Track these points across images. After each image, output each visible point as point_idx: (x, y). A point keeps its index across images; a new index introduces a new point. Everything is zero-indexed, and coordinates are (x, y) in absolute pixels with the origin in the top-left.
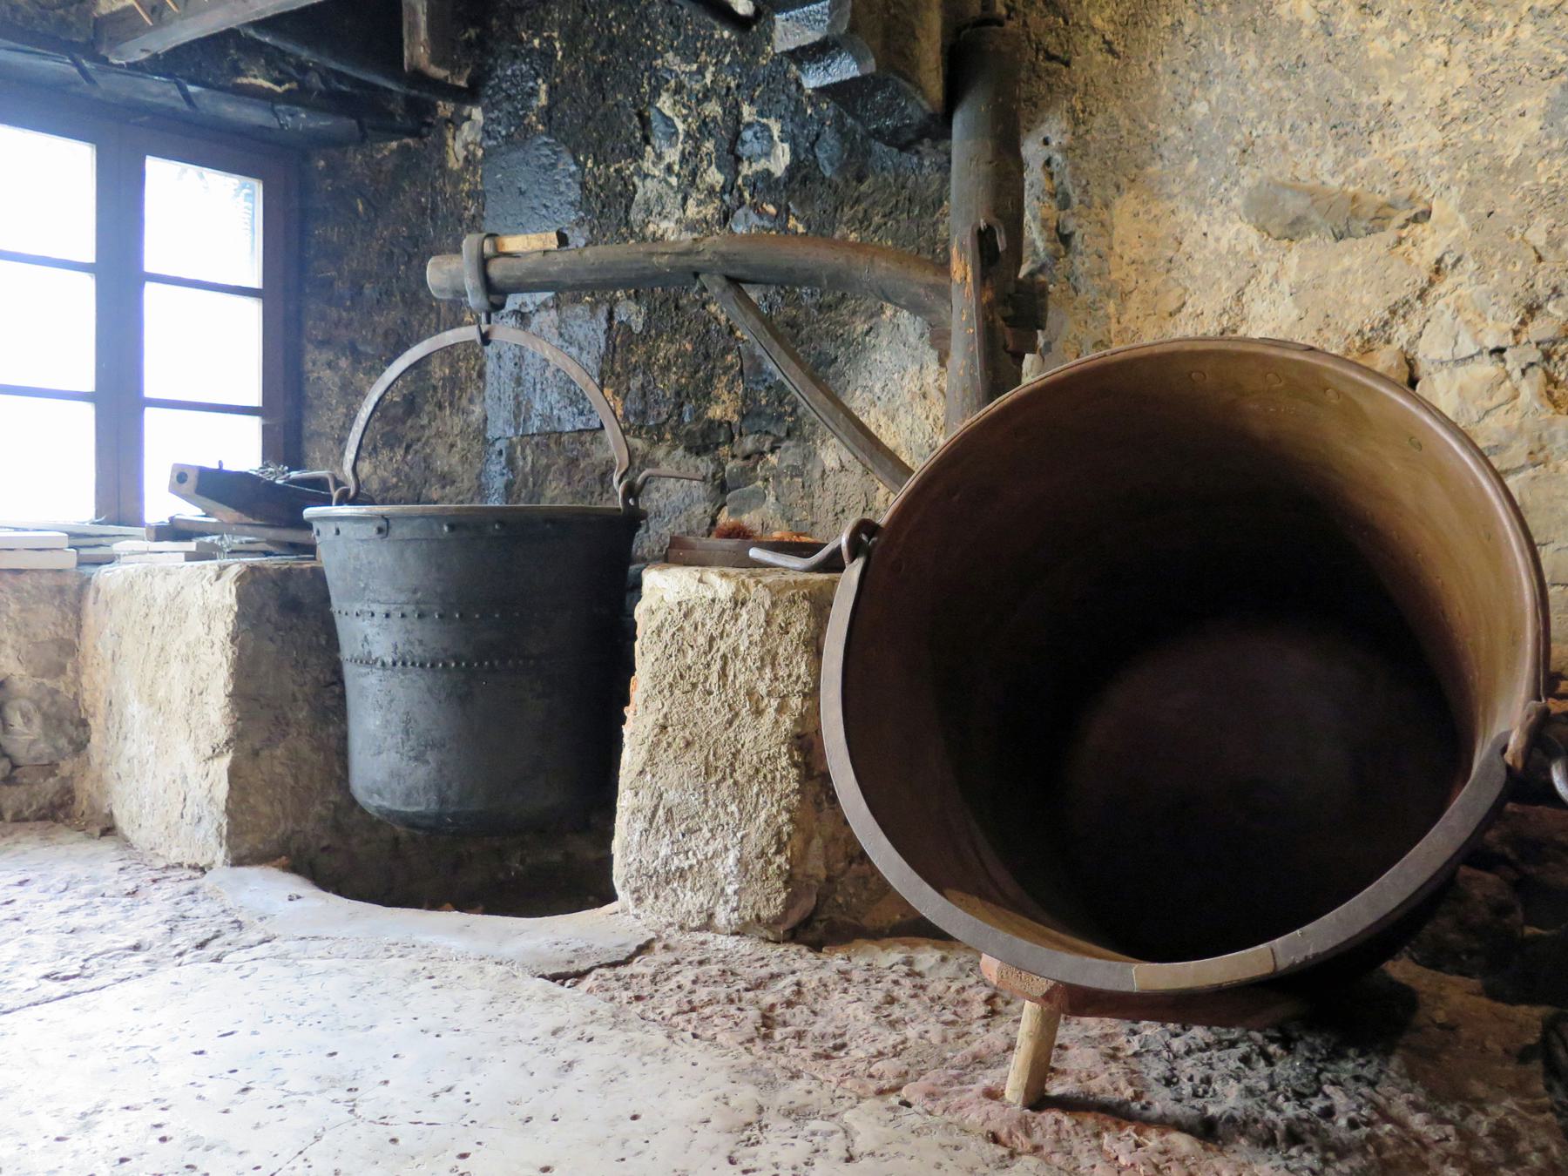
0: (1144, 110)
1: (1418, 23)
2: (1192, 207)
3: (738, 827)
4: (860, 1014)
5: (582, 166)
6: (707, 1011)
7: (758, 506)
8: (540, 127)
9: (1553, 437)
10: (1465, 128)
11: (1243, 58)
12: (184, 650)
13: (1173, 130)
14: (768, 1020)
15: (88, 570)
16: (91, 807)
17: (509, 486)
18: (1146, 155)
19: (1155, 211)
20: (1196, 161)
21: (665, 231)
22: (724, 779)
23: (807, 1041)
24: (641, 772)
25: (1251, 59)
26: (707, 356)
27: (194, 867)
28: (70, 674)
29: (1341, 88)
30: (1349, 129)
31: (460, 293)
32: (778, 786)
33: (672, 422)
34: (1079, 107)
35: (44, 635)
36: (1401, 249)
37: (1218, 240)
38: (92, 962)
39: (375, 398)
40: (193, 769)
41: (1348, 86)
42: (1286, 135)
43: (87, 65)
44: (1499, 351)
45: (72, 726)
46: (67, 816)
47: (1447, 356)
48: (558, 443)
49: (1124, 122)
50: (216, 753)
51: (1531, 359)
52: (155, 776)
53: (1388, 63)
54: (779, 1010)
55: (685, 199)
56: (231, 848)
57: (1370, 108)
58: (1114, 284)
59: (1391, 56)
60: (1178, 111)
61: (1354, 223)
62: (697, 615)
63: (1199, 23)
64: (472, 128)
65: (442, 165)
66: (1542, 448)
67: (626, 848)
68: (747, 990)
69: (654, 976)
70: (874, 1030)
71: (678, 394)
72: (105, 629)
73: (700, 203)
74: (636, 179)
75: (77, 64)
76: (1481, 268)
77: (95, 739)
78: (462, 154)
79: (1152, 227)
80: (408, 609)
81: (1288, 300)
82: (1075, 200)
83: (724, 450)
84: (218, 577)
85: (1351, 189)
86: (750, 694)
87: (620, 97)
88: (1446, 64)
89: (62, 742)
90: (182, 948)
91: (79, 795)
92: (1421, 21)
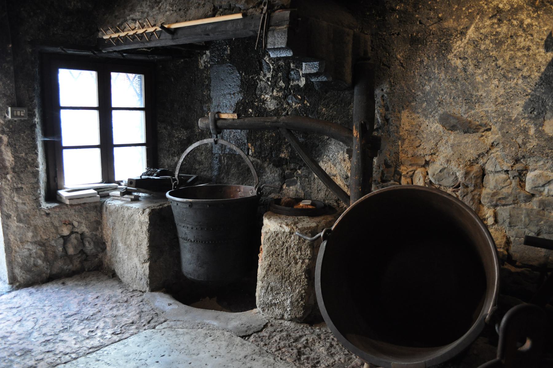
1: (491, 73)
2: (424, 117)
3: (291, 293)
4: (323, 351)
6: (283, 350)
9: (520, 197)
10: (502, 106)
11: (440, 75)
12: (134, 232)
13: (419, 93)
14: (300, 353)
15: (103, 200)
16: (108, 266)
17: (220, 168)
18: (411, 99)
19: (413, 117)
21: (267, 98)
22: (287, 280)
23: (310, 361)
24: (264, 277)
25: (442, 76)
26: (280, 138)
27: (141, 291)
31: (208, 129)
34: (392, 81)
35: (92, 220)
36: (482, 138)
37: (431, 128)
38: (123, 328)
39: (184, 157)
40: (139, 265)
42: (452, 100)
44: (507, 172)
45: (101, 244)
47: (493, 170)
48: (234, 157)
49: (405, 88)
50: (145, 262)
51: (515, 175)
52: (128, 265)
53: (482, 83)
54: (302, 349)
55: (273, 90)
57: (476, 96)
58: (400, 136)
59: (482, 82)
60: (421, 88)
61: (470, 130)
62: (280, 235)
64: (206, 57)
65: (198, 66)
66: (517, 200)
67: (260, 297)
68: (294, 342)
69: (269, 336)
70: (327, 357)
71: (271, 148)
72: (108, 221)
76: (504, 147)
77: (108, 248)
78: (203, 65)
79: (412, 121)
80: (198, 227)
82: (390, 109)
84: (143, 213)
86: (294, 258)
87: (253, 55)
88: (498, 87)
89: (99, 249)
92: (491, 73)
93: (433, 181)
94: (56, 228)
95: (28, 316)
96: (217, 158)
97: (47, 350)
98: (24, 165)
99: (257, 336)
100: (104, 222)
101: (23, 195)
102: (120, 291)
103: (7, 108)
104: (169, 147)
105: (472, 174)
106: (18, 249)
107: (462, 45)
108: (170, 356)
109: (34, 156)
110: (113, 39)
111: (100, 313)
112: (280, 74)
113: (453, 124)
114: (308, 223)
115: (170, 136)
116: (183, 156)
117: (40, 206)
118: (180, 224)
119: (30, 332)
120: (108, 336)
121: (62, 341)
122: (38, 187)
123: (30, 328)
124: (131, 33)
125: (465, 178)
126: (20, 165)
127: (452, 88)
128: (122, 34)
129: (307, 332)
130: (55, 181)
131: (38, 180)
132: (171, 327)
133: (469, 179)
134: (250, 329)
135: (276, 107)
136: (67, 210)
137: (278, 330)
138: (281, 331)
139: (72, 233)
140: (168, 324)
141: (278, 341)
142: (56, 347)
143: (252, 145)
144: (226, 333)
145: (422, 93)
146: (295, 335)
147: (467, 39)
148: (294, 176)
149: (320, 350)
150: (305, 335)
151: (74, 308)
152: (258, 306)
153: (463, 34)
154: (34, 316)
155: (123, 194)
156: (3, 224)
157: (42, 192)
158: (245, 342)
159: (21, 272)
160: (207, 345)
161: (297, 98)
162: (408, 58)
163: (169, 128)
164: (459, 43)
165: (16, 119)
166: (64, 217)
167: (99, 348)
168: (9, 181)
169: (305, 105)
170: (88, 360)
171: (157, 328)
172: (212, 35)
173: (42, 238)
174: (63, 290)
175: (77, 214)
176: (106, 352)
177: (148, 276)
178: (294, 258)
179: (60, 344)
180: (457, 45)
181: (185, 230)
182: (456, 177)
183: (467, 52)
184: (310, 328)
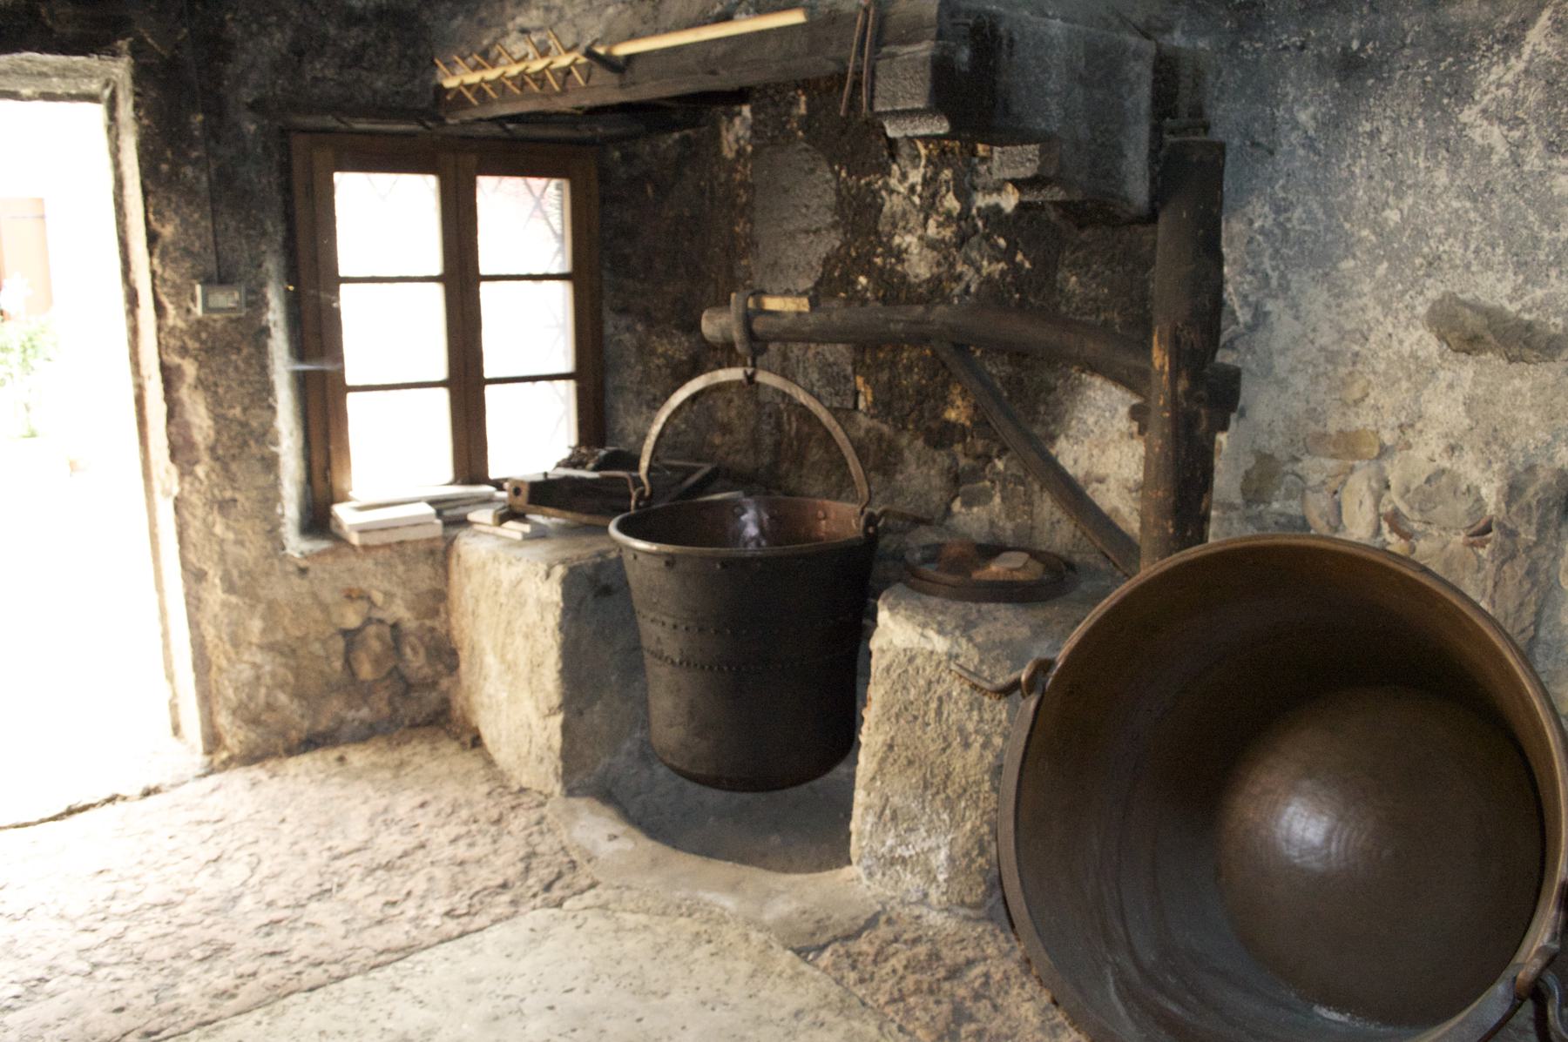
0: (1340, 210)
2: (1379, 308)
5: (837, 175)
6: (912, 1000)
7: (986, 503)
8: (800, 133)
11: (1435, 174)
13: (1365, 233)
15: (453, 531)
17: (778, 444)
20: (1385, 265)
21: (909, 245)
22: (938, 793)
24: (873, 779)
25: (1442, 178)
27: (540, 793)
28: (443, 615)
29: (1525, 218)
30: (1529, 259)
32: (981, 804)
33: (914, 415)
35: (424, 586)
37: (1401, 342)
38: (476, 899)
40: (535, 720)
41: (1531, 219)
43: (430, 124)
45: (446, 654)
46: (432, 552)
50: (552, 712)
55: (926, 219)
56: (565, 783)
60: (1372, 216)
62: (919, 661)
63: (1397, 134)
68: (946, 979)
69: (877, 955)
71: (918, 393)
73: (939, 225)
74: (884, 193)
75: (422, 124)
81: (1461, 408)
83: (958, 448)
85: (1527, 317)
89: (440, 667)
90: (535, 890)
91: (453, 704)
93: (1404, 509)
94: (325, 608)
95: (238, 849)
96: (770, 416)
97: (269, 950)
98: (240, 439)
99: (842, 951)
100: (454, 593)
101: (237, 520)
102: (485, 788)
103: (193, 287)
104: (640, 383)
105: (1531, 490)
106: (224, 663)
107: (1509, 78)
108: (587, 992)
109: (266, 414)
110: (469, 87)
111: (421, 853)
112: (947, 174)
113: (1472, 332)
114: (1008, 622)
115: (643, 350)
116: (663, 416)
117: (284, 548)
118: (644, 612)
119: (235, 893)
120: (434, 921)
121: (313, 925)
122: (278, 498)
123: (237, 883)
124: (514, 70)
125: (1508, 504)
126: (230, 438)
127: (1472, 215)
128: (491, 74)
129: (990, 951)
130: (326, 478)
131: (277, 477)
132: (604, 907)
133: (1521, 509)
134: (826, 929)
135: (935, 270)
136: (353, 559)
137: (906, 936)
138: (916, 941)
139: (368, 621)
140: (598, 896)
141: (901, 971)
142: (293, 942)
143: (867, 382)
144: (754, 935)
145: (1374, 233)
146: (950, 956)
147: (1525, 57)
148: (985, 478)
149: (1022, 1010)
150: (985, 959)
151: (358, 832)
152: (854, 860)
153: (1511, 42)
154: (253, 849)
155: (502, 519)
156: (187, 595)
157: (290, 509)
158: (804, 967)
159: (233, 723)
160: (696, 967)
161: (995, 246)
162: (1332, 124)
163: (639, 327)
164: (1497, 71)
165: (216, 316)
166: (347, 581)
167: (407, 951)
168: (201, 482)
169: (1016, 268)
170: (371, 986)
171: (567, 905)
172: (724, 73)
173: (287, 634)
174: (337, 780)
175: (380, 569)
176: (419, 968)
177: (558, 752)
178: (961, 730)
179: (304, 934)
180: (1493, 77)
181: (656, 630)
182: (1479, 499)
183: (1525, 98)
184: (1002, 937)
